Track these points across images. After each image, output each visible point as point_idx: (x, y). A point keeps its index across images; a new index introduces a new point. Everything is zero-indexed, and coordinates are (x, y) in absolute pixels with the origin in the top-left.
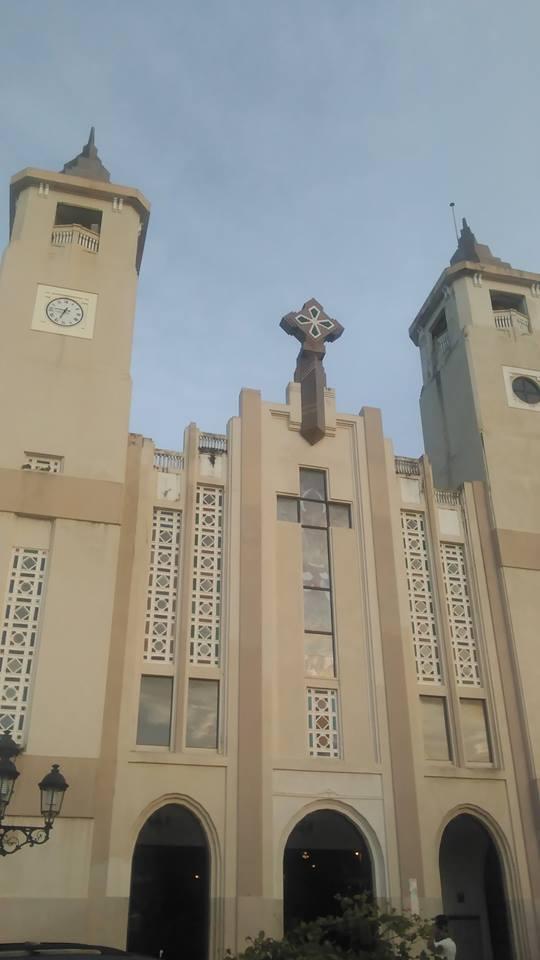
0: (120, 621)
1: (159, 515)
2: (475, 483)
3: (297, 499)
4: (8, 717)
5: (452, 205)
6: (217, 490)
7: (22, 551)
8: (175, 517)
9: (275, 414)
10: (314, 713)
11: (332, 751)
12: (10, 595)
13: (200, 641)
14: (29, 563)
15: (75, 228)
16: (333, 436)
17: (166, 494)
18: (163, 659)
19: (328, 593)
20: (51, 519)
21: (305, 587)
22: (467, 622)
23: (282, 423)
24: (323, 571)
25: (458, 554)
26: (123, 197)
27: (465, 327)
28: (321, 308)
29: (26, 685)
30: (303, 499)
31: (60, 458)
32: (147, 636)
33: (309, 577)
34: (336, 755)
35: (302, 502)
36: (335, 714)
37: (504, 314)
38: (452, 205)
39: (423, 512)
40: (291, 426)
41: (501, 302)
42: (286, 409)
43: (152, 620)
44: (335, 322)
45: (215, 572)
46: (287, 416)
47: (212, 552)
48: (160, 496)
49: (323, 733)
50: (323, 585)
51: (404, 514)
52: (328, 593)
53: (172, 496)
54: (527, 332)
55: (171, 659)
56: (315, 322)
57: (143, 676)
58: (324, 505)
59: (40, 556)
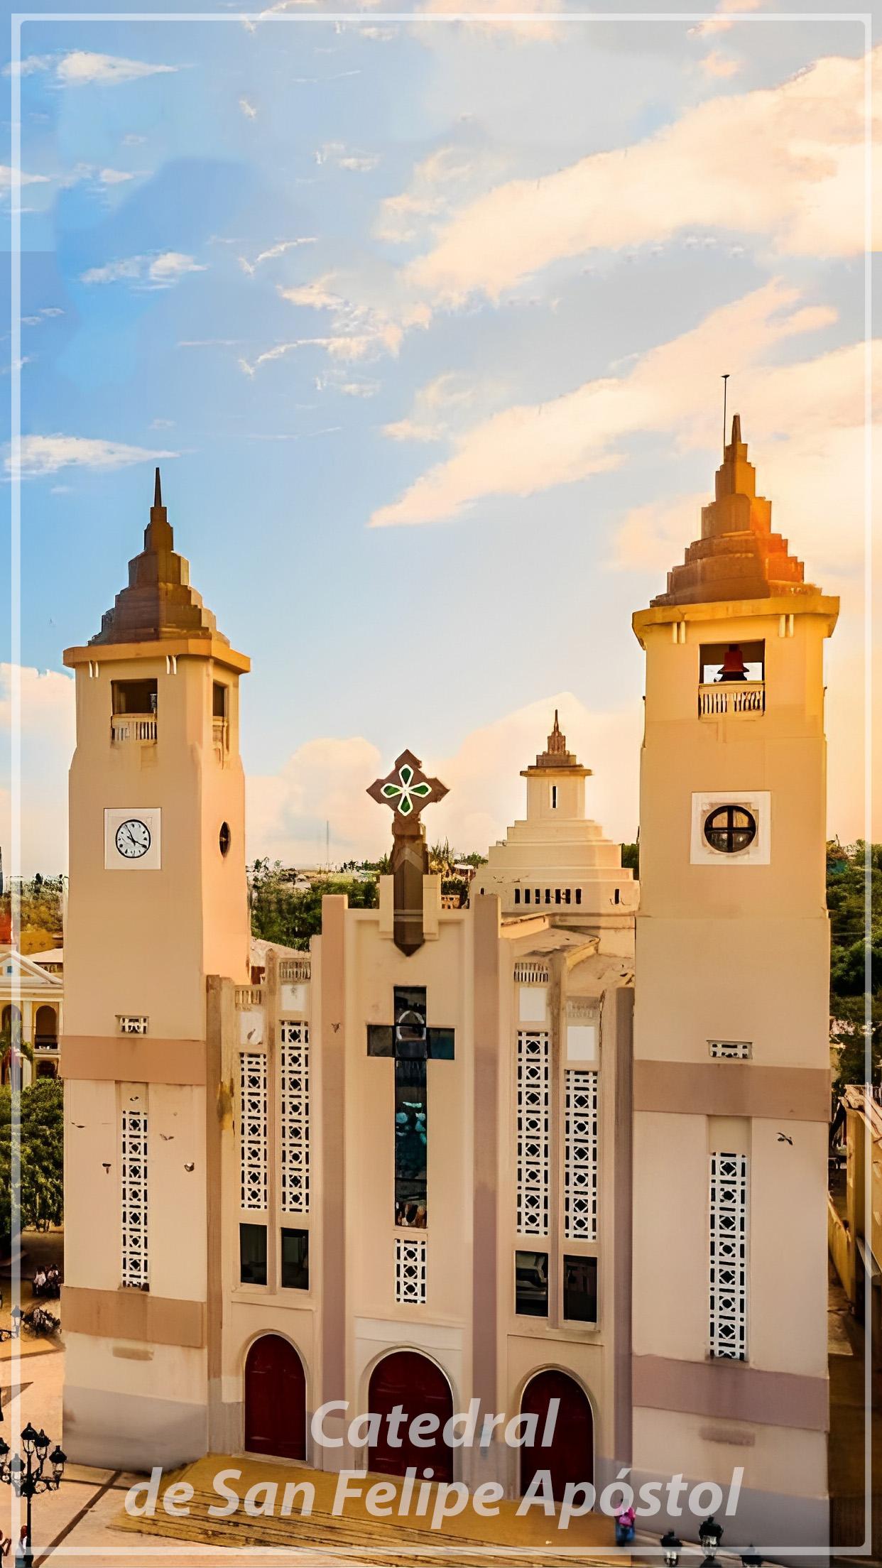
1: (246, 1059)
5: (726, 377)
8: (591, 1078)
10: (402, 1262)
12: (283, 1164)
13: (575, 1214)
14: (728, 1168)
17: (250, 1035)
20: (147, 1083)
32: (594, 1216)
38: (726, 377)
48: (244, 1039)
53: (257, 1038)
57: (518, 1252)
59: (739, 1160)
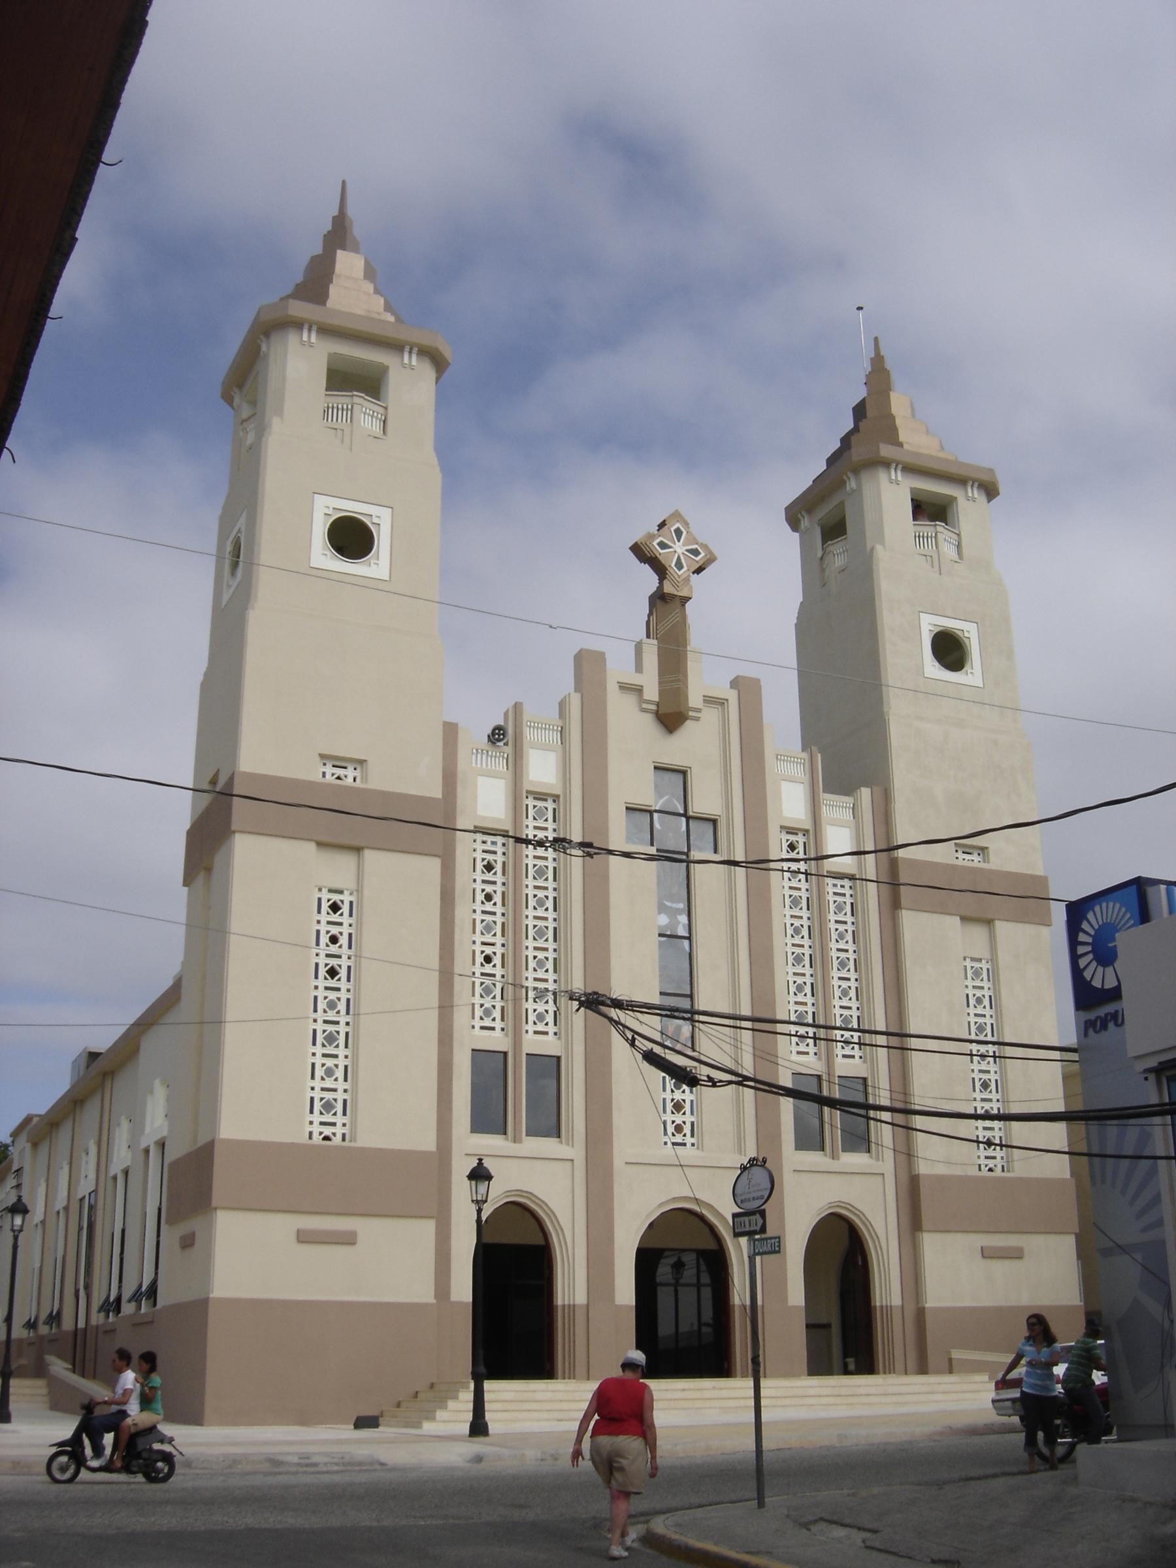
0: (446, 1009)
2: (875, 788)
3: (651, 813)
4: (322, 1106)
6: (550, 801)
7: (325, 891)
9: (624, 687)
11: (689, 1140)
13: (535, 1006)
15: (356, 400)
16: (697, 719)
18: (493, 1029)
19: (686, 943)
21: (660, 935)
22: (849, 923)
23: (630, 700)
24: (679, 912)
25: (847, 887)
26: (417, 345)
27: (872, 549)
28: (686, 524)
29: (346, 1096)
30: (656, 811)
31: (362, 762)
33: (663, 920)
34: (693, 1145)
35: (656, 815)
36: (693, 1119)
37: (926, 528)
38: (860, 308)
39: (807, 831)
40: (644, 706)
41: (929, 510)
42: (636, 679)
43: (478, 948)
44: (705, 547)
45: (551, 915)
46: (638, 690)
47: (546, 888)
49: (679, 1119)
50: (682, 931)
51: (784, 833)
52: (686, 943)
54: (956, 557)
55: (503, 1029)
56: (680, 548)
58: (684, 819)
